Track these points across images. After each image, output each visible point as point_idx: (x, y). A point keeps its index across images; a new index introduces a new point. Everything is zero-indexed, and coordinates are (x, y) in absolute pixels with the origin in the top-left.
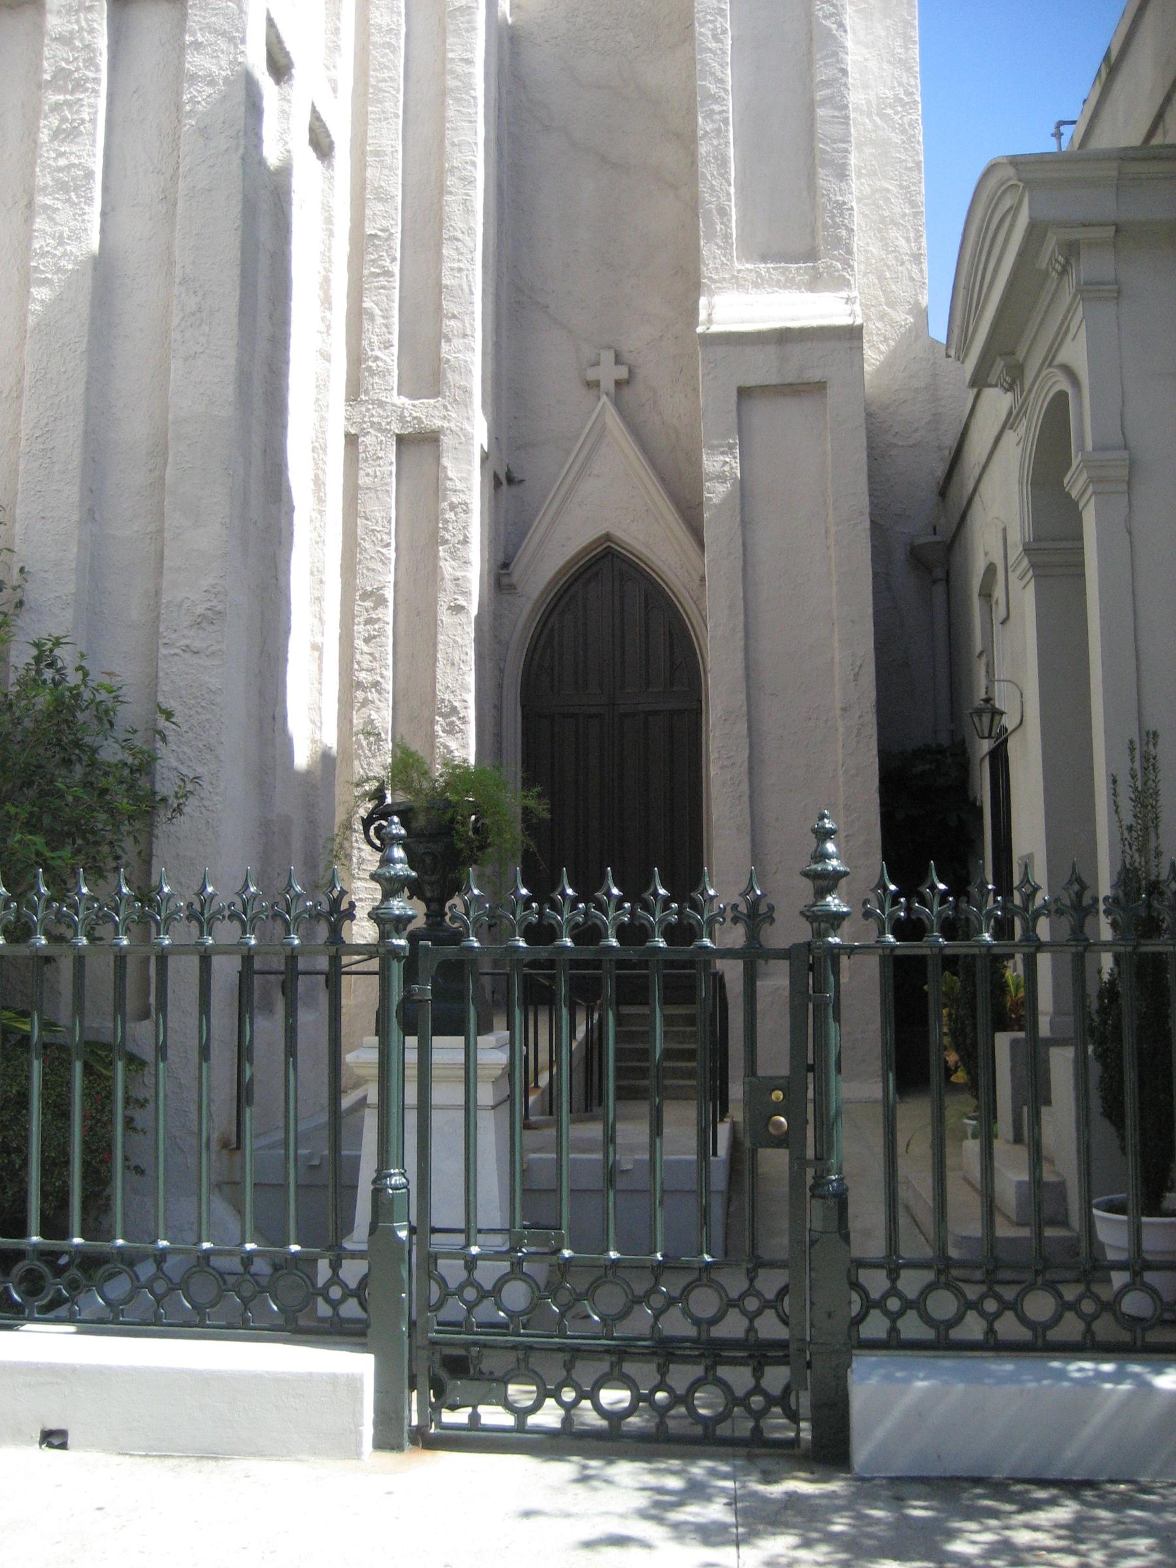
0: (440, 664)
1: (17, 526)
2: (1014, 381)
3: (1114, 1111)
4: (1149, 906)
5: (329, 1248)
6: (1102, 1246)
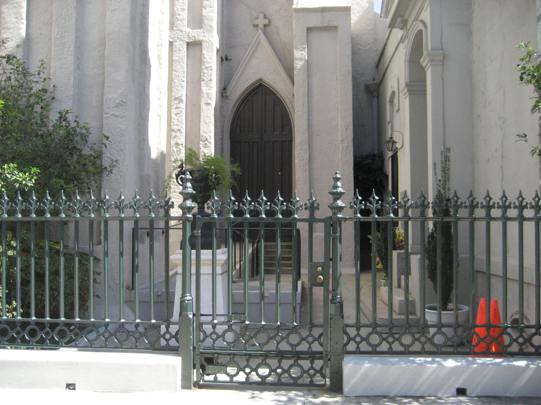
0: (202, 123)
1: (52, 71)
2: (404, 26)
3: (433, 276)
4: (447, 205)
5: (165, 321)
6: (427, 321)
